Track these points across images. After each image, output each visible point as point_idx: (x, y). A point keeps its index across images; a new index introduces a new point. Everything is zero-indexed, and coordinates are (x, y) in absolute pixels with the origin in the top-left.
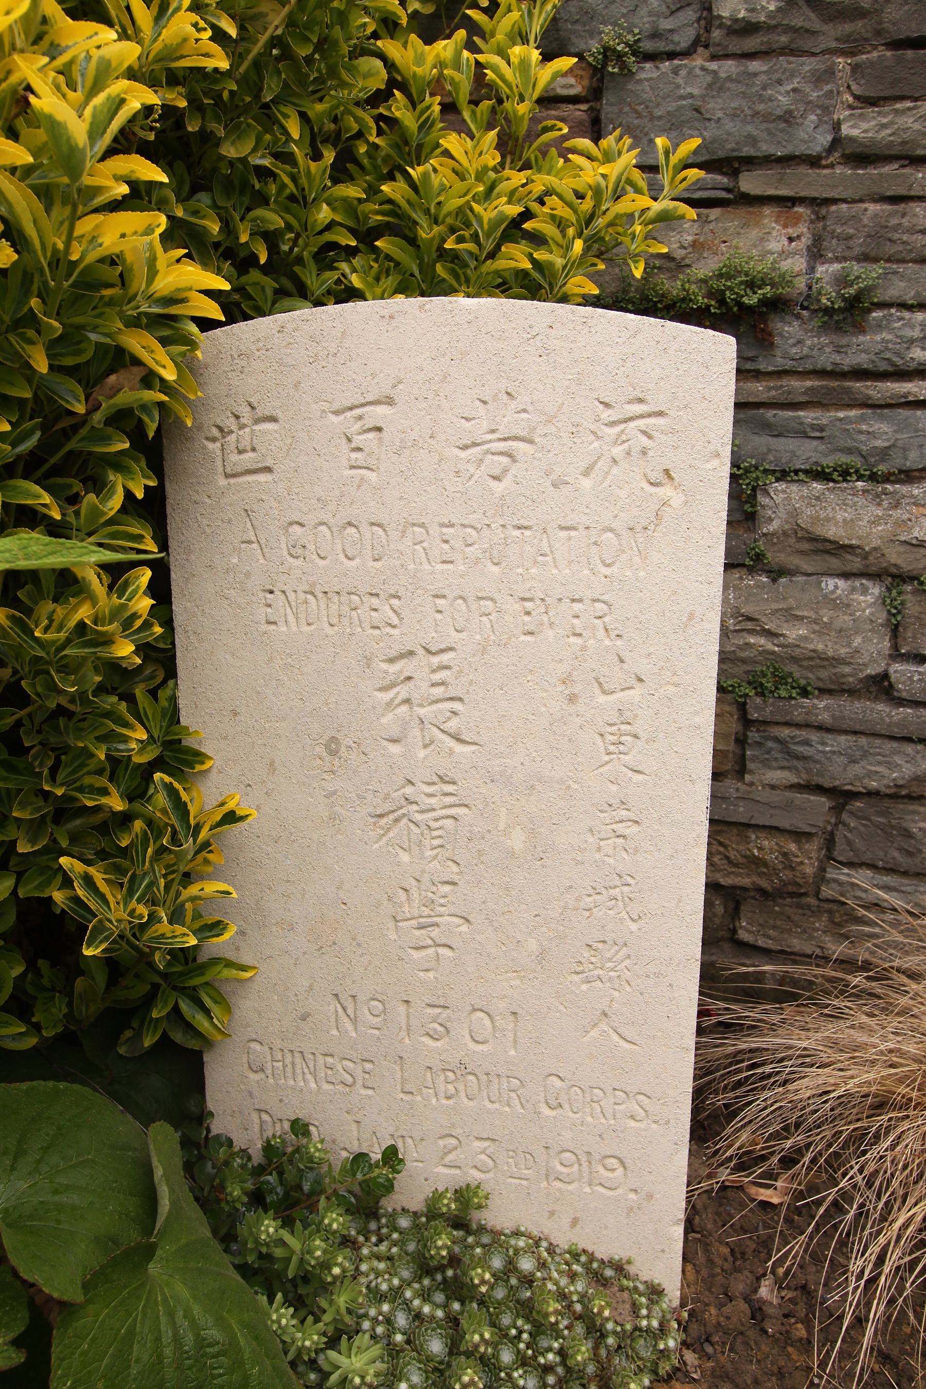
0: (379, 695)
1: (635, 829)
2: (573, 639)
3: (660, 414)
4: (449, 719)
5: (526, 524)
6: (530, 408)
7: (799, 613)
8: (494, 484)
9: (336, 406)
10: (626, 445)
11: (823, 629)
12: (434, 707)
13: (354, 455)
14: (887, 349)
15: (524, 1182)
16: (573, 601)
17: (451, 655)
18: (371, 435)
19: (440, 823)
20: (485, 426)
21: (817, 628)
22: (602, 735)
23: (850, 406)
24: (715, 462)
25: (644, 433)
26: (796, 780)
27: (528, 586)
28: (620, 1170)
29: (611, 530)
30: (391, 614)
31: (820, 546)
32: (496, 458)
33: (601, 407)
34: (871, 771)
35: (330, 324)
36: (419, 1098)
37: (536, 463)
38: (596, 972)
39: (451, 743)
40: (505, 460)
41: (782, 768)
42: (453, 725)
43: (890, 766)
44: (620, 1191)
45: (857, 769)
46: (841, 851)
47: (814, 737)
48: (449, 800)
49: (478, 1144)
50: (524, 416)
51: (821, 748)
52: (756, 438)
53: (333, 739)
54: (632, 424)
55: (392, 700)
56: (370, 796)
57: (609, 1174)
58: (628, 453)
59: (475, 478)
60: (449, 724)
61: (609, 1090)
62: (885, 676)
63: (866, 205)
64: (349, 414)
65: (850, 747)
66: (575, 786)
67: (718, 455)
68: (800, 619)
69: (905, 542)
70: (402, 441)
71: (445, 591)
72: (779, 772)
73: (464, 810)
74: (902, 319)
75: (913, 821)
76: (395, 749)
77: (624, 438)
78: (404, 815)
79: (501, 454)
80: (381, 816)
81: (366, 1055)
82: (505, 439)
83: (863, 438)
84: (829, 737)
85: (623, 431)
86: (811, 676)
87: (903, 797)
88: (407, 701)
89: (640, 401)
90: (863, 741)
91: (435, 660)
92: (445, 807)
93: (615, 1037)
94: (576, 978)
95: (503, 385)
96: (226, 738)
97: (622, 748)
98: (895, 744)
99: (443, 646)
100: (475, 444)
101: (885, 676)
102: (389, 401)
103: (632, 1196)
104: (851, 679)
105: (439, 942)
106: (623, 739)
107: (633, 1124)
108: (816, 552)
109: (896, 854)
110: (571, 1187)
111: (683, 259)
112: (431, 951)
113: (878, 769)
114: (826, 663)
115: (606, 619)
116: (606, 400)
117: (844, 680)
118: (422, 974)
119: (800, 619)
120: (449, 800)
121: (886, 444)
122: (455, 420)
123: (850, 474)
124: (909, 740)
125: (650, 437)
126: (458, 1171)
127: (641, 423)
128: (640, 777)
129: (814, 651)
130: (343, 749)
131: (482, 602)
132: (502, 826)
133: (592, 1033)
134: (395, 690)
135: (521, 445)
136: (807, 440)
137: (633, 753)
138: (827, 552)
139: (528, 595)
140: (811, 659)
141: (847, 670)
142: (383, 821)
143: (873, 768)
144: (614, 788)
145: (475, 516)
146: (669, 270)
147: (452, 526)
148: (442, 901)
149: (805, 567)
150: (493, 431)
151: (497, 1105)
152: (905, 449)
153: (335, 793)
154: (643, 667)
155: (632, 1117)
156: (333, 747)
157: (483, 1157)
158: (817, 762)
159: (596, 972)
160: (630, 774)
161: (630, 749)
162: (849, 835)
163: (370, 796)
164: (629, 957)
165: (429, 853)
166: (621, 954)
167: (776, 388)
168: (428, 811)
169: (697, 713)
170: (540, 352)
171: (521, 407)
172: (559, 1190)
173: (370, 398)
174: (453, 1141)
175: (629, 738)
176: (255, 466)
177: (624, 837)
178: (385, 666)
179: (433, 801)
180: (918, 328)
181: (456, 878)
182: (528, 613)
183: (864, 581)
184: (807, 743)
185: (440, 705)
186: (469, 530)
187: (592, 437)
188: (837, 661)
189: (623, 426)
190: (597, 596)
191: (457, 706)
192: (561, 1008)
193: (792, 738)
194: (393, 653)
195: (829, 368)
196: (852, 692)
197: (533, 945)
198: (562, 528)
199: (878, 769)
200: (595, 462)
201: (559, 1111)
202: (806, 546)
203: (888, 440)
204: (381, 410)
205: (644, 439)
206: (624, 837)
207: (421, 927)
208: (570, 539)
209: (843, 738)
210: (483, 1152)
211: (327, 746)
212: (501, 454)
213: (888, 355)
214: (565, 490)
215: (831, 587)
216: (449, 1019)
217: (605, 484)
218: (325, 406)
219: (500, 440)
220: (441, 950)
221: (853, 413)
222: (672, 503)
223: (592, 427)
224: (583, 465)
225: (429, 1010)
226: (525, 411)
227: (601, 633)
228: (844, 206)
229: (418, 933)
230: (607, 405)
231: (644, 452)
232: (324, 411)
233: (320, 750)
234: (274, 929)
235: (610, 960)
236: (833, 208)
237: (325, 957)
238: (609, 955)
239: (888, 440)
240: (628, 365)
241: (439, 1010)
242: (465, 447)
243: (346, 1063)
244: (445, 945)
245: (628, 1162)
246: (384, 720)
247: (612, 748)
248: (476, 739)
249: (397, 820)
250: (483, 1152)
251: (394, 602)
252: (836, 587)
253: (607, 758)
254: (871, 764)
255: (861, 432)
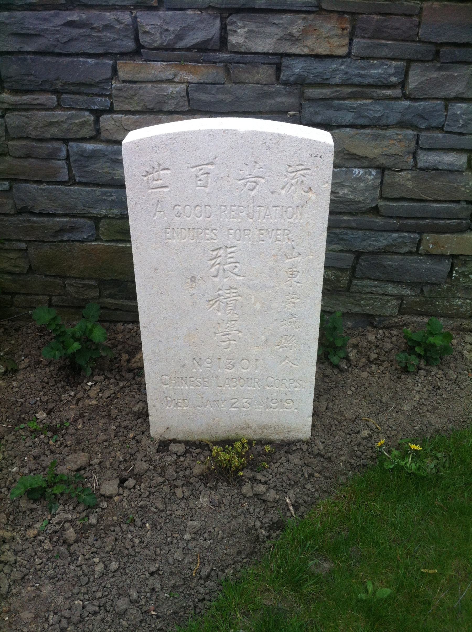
0: (210, 262)
1: (298, 300)
2: (277, 242)
3: (308, 169)
4: (234, 269)
5: (262, 205)
6: (263, 167)
7: (344, 184)
8: (250, 192)
9: (193, 165)
10: (296, 179)
11: (354, 190)
12: (229, 265)
13: (199, 182)
14: (381, 77)
15: (260, 410)
16: (277, 230)
17: (235, 248)
18: (205, 175)
19: (231, 302)
20: (247, 173)
21: (351, 189)
22: (287, 272)
23: (366, 98)
24: (326, 185)
25: (303, 175)
26: (342, 248)
27: (262, 225)
28: (292, 403)
29: (291, 207)
30: (213, 235)
31: (353, 156)
32: (251, 184)
33: (288, 167)
34: (370, 244)
35: (190, 137)
36: (224, 388)
37: (265, 185)
38: (285, 345)
39: (235, 276)
40: (254, 184)
41: (336, 244)
42: (236, 270)
43: (378, 241)
44: (292, 409)
45: (365, 243)
46: (358, 274)
47: (349, 232)
48: (234, 294)
49: (244, 400)
50: (261, 169)
51: (352, 236)
52: (328, 112)
53: (193, 277)
54: (299, 173)
55: (214, 263)
56: (206, 295)
57: (289, 405)
58: (297, 182)
59: (244, 190)
60: (234, 271)
61: (288, 380)
62: (377, 207)
63: (374, 16)
64: (197, 168)
65: (363, 235)
66: (278, 288)
67: (327, 182)
68: (345, 186)
69: (386, 155)
70: (218, 178)
71: (233, 228)
72: (335, 246)
73: (240, 298)
74: (387, 65)
75: (385, 261)
76: (215, 279)
77: (296, 177)
78: (218, 300)
79: (253, 182)
80: (210, 301)
81: (205, 376)
82: (254, 177)
83: (371, 112)
84: (354, 232)
85: (295, 175)
86: (348, 208)
87: (383, 252)
88: (219, 264)
89: (302, 165)
90: (367, 233)
91: (230, 250)
92: (233, 297)
93: (291, 364)
94: (278, 347)
95: (254, 159)
96: (153, 278)
97: (293, 276)
98: (380, 233)
99: (232, 246)
100: (243, 179)
101: (377, 207)
102: (212, 164)
103: (296, 410)
104: (364, 209)
105: (231, 339)
106: (294, 273)
107: (296, 389)
108: (351, 159)
109: (379, 274)
110: (276, 410)
111: (299, 37)
112: (228, 342)
113: (373, 243)
114: (354, 203)
115: (289, 236)
116: (290, 165)
117: (361, 209)
118: (225, 350)
119: (345, 186)
120: (234, 294)
121: (380, 115)
122: (237, 171)
123: (384, 372)
124: (384, 231)
125: (304, 177)
126: (237, 409)
127: (302, 172)
128: (299, 285)
129: (349, 199)
130: (197, 280)
131: (246, 231)
132: (253, 302)
133: (283, 363)
134: (215, 260)
135: (260, 179)
136: (349, 113)
137: (298, 277)
138: (356, 159)
139: (262, 229)
140: (348, 202)
141: (362, 205)
142: (211, 302)
143: (371, 243)
144: (291, 288)
145: (244, 203)
146: (292, 41)
147: (235, 206)
148: (232, 326)
149: (347, 165)
150: (250, 175)
151: (251, 388)
152: (387, 117)
153: (194, 294)
154: (301, 250)
155: (296, 387)
156: (193, 279)
157: (246, 404)
158: (350, 241)
159: (285, 345)
160: (296, 284)
161: (296, 276)
162: (362, 268)
163: (206, 295)
164: (295, 339)
165: (228, 312)
166: (293, 339)
167: (336, 91)
168: (227, 298)
169: (319, 264)
170: (267, 148)
171: (260, 167)
172: (272, 411)
173: (205, 162)
174: (236, 400)
175: (296, 273)
176: (162, 186)
177: (294, 303)
178: (211, 253)
179: (228, 295)
180: (393, 69)
181: (237, 319)
182: (262, 234)
183: (370, 170)
184: (346, 234)
185: (231, 265)
186: (241, 207)
187: (285, 177)
188: (360, 202)
189: (295, 173)
190: (285, 228)
191: (237, 265)
192: (273, 356)
193: (341, 233)
194: (214, 248)
195: (357, 83)
196: (364, 213)
197: (263, 338)
198: (274, 207)
199: (373, 243)
200: (286, 185)
201: (272, 387)
202: (348, 156)
203: (381, 113)
204: (210, 167)
205: (302, 177)
206: (294, 303)
207: (225, 335)
208: (276, 210)
209: (360, 232)
210: (246, 402)
211: (191, 280)
212: (253, 182)
213: (381, 79)
214: (275, 194)
215: (357, 173)
216: (234, 363)
217: (289, 192)
218: (189, 165)
219: (252, 177)
220: (231, 342)
221: (368, 101)
222: (312, 198)
223: (285, 174)
224: (282, 186)
225: (228, 361)
226: (261, 168)
227: (287, 240)
228: (365, 16)
229: (224, 337)
230: (290, 166)
231: (302, 182)
232: (188, 167)
233: (188, 280)
234: (172, 339)
235: (289, 341)
236: (360, 16)
237: (191, 347)
238: (289, 339)
239: (381, 113)
240: (298, 153)
241: (231, 360)
242: (240, 180)
243: (198, 379)
244: (233, 340)
245: (294, 400)
246: (211, 270)
247: (290, 276)
248: (244, 275)
249: (216, 302)
250: (246, 402)
251: (214, 231)
252: (359, 173)
253: (289, 279)
254: (371, 241)
255: (370, 110)
